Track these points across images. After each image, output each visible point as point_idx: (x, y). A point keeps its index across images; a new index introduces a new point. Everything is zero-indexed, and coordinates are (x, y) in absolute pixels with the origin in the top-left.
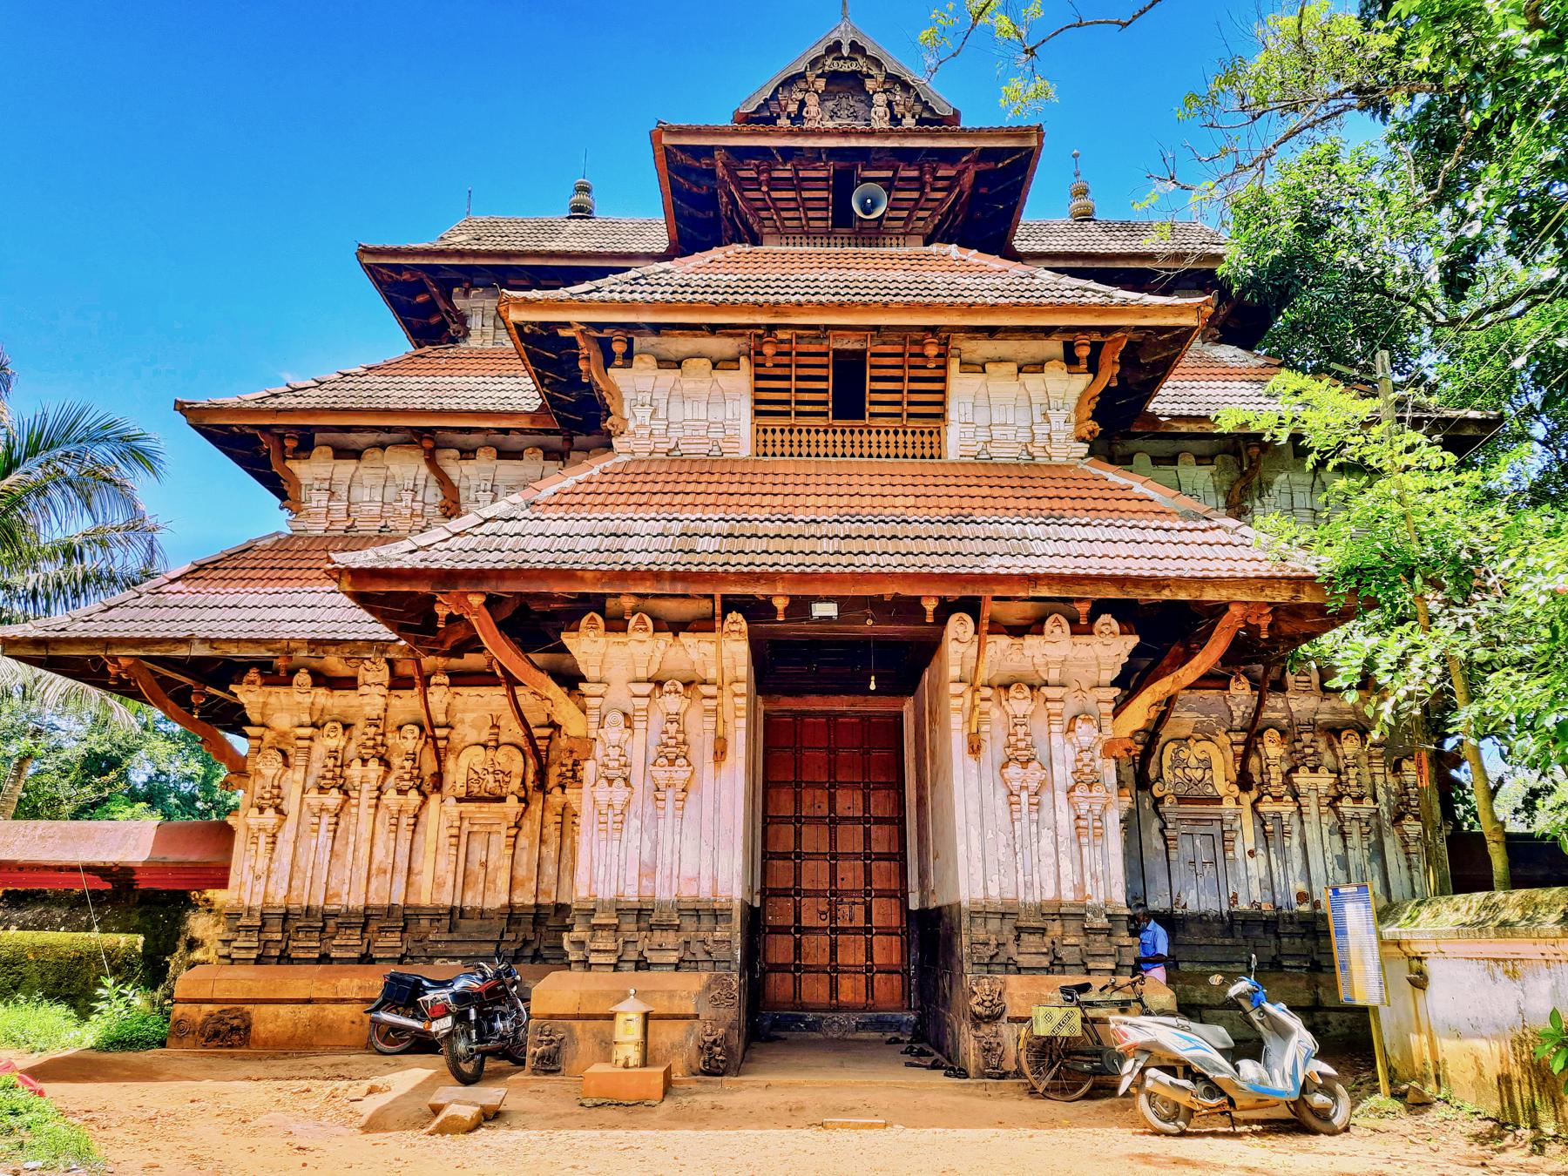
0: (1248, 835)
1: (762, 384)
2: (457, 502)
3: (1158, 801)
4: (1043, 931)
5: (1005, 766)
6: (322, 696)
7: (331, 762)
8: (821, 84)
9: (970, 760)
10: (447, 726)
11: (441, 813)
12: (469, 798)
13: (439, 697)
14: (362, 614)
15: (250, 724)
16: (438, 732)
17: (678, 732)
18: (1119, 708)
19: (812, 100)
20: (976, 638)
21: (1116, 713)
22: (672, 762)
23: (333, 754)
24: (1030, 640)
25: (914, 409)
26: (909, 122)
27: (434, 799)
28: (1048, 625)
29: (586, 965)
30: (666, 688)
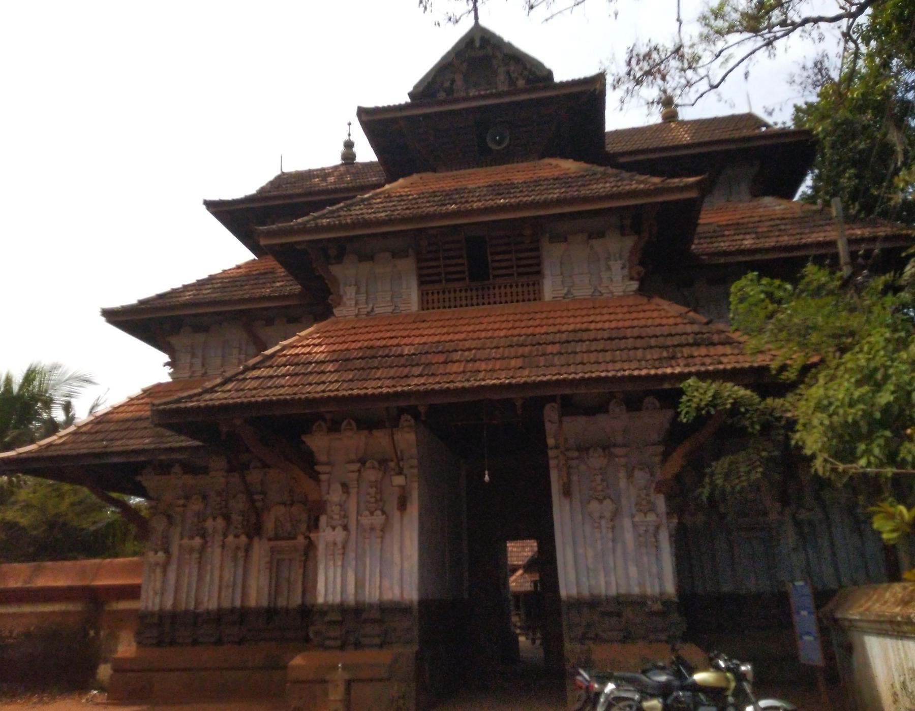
0: (790, 538)
3: (723, 516)
4: (619, 615)
6: (189, 480)
9: (566, 502)
11: (260, 550)
12: (277, 538)
16: (256, 497)
17: (376, 493)
18: (666, 456)
22: (372, 513)
24: (601, 418)
25: (521, 270)
26: (521, 83)
27: (256, 540)
28: (611, 406)
30: (368, 465)
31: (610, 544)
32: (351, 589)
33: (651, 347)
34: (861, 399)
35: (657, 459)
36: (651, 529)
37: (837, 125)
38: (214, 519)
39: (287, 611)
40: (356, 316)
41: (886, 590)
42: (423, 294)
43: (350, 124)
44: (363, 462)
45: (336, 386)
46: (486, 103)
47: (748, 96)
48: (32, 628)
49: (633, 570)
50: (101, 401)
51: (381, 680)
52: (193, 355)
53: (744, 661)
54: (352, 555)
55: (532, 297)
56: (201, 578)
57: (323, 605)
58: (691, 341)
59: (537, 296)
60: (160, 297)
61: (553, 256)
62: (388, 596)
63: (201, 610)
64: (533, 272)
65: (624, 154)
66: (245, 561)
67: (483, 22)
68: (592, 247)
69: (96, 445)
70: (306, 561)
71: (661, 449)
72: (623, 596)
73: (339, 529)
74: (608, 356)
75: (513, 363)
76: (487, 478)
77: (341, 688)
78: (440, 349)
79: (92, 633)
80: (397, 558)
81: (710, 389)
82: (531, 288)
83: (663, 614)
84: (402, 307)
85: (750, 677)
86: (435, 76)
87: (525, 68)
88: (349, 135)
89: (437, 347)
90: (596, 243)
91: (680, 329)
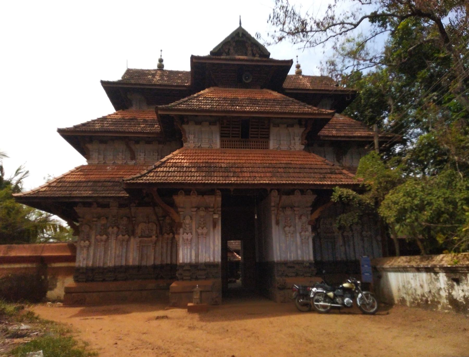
0: (340, 242)
1: (223, 129)
2: (135, 156)
5: (284, 227)
6: (100, 210)
7: (103, 228)
8: (234, 44)
10: (135, 217)
11: (134, 243)
13: (133, 210)
14: (217, 227)
15: (80, 217)
18: (312, 212)
19: (232, 48)
20: (279, 196)
21: (311, 214)
22: (202, 228)
23: (103, 225)
29: (182, 279)
30: (201, 209)
31: (292, 243)
32: (193, 258)
33: (316, 173)
34: (409, 202)
35: (309, 212)
36: (307, 237)
37: (367, 91)
38: (113, 228)
39: (146, 267)
40: (194, 147)
41: (398, 258)
42: (222, 141)
43: (161, 51)
44: (198, 208)
45: (201, 178)
46: (239, 61)
47: (240, 17)
48: (10, 275)
49: (299, 252)
50: (22, 168)
51: (209, 291)
52: (99, 154)
53: (358, 280)
54: (194, 244)
55: (265, 147)
56: (105, 253)
57: (182, 263)
58: (329, 172)
59: (267, 147)
60: (83, 125)
61: (274, 131)
62: (208, 260)
63: (105, 267)
64: (265, 137)
65: (287, 89)
66: (127, 246)
67: (243, 26)
68: (288, 130)
69: (63, 193)
70: (155, 247)
71: (311, 209)
72: (295, 261)
73: (190, 234)
74: (302, 175)
75: (268, 174)
76: (256, 217)
77: (199, 294)
78: (237, 166)
79: (43, 277)
80: (212, 246)
81: (345, 191)
82: (265, 144)
83: (309, 267)
84: (213, 146)
85: (360, 285)
86: (222, 47)
87: (260, 50)
88: (161, 56)
89: (235, 165)
90: (290, 129)
91: (323, 166)
